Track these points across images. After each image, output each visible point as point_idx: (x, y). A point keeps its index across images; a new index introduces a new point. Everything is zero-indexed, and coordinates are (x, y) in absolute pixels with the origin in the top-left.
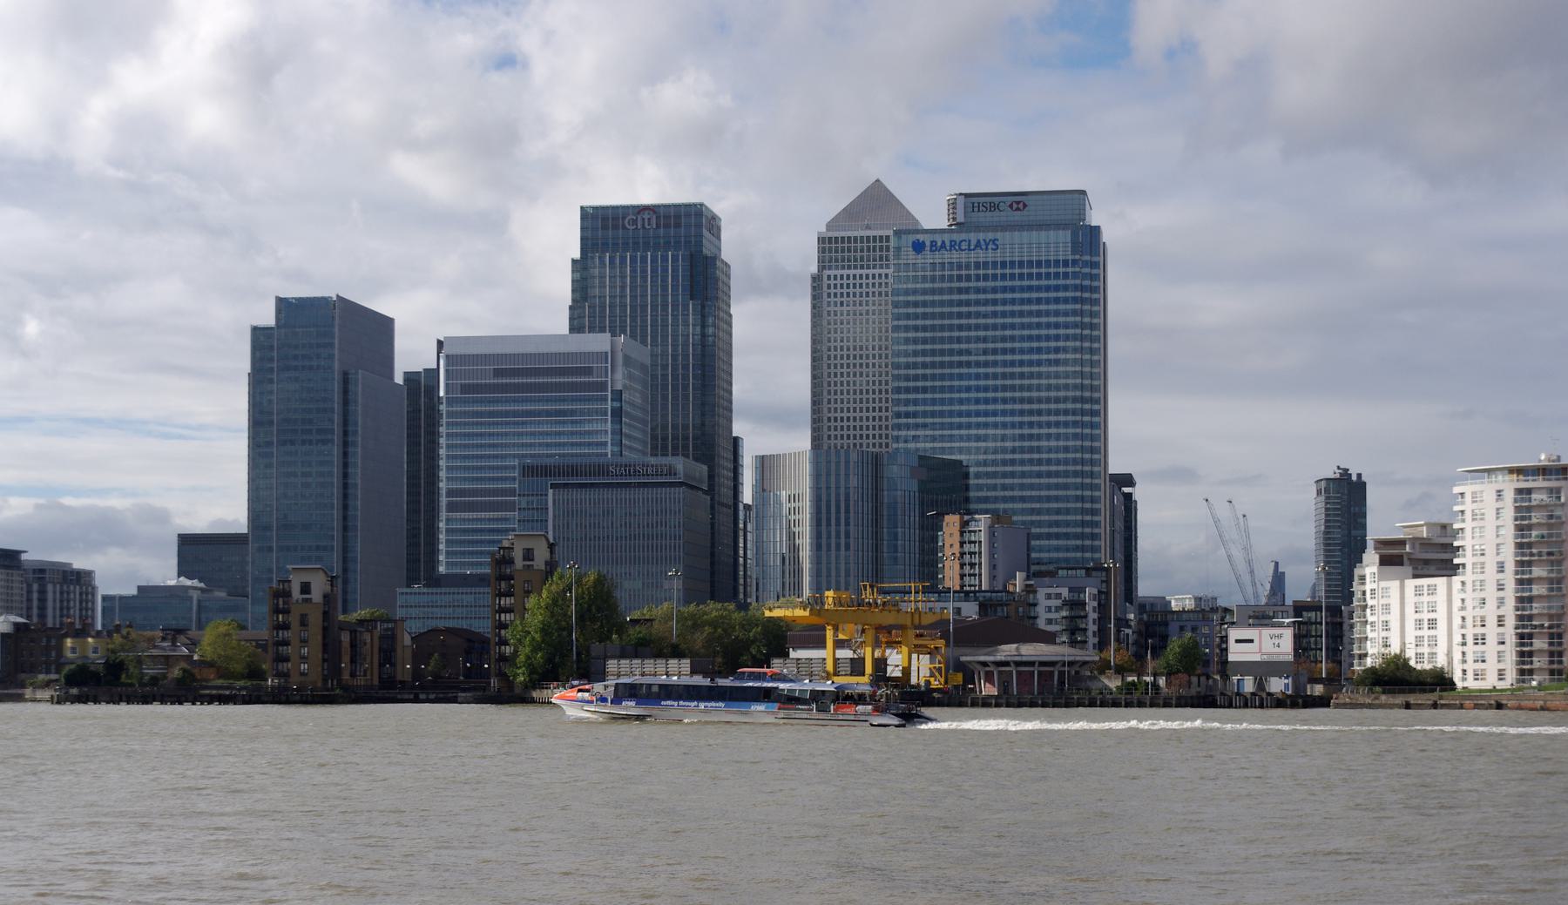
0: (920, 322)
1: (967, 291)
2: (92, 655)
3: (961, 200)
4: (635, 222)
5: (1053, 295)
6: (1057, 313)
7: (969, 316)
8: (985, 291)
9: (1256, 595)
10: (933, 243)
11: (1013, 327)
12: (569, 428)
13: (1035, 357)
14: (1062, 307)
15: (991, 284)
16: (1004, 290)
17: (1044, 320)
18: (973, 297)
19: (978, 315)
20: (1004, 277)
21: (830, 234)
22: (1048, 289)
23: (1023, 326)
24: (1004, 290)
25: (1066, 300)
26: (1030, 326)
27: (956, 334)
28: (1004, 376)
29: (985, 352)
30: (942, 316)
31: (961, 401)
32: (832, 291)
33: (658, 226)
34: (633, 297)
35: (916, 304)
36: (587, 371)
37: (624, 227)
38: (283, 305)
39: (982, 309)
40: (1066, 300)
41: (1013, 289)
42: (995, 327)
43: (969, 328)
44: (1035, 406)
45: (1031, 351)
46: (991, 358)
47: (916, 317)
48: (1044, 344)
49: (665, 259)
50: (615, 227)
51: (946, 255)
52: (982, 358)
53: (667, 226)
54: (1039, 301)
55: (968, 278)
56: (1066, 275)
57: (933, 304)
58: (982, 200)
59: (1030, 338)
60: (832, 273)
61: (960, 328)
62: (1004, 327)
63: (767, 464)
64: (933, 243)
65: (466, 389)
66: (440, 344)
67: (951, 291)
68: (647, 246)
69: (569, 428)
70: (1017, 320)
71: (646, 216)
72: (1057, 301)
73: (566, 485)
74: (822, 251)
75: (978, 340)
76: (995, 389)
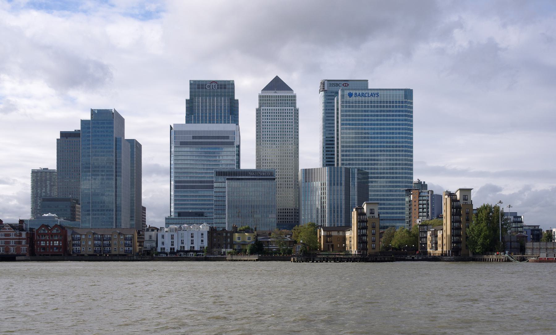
0: (351, 122)
1: (367, 111)
2: (247, 240)
3: (326, 82)
4: (209, 86)
5: (398, 113)
7: (368, 120)
10: (356, 94)
13: (391, 136)
14: (401, 118)
15: (376, 109)
16: (381, 111)
17: (395, 122)
18: (370, 113)
19: (371, 120)
20: (381, 106)
21: (263, 94)
22: (396, 111)
23: (387, 124)
24: (381, 111)
25: (402, 116)
27: (364, 127)
28: (381, 142)
29: (374, 133)
30: (359, 120)
32: (264, 114)
33: (218, 88)
34: (210, 114)
36: (228, 137)
37: (206, 88)
39: (373, 118)
40: (402, 116)
41: (384, 111)
43: (368, 124)
45: (390, 133)
46: (376, 136)
47: (350, 120)
49: (213, 100)
51: (360, 98)
52: (373, 136)
54: (393, 116)
55: (368, 107)
58: (333, 82)
59: (390, 129)
61: (365, 124)
63: (307, 172)
64: (356, 94)
66: (171, 128)
67: (362, 111)
70: (385, 122)
71: (214, 85)
74: (260, 100)
75: (372, 129)
76: (377, 147)
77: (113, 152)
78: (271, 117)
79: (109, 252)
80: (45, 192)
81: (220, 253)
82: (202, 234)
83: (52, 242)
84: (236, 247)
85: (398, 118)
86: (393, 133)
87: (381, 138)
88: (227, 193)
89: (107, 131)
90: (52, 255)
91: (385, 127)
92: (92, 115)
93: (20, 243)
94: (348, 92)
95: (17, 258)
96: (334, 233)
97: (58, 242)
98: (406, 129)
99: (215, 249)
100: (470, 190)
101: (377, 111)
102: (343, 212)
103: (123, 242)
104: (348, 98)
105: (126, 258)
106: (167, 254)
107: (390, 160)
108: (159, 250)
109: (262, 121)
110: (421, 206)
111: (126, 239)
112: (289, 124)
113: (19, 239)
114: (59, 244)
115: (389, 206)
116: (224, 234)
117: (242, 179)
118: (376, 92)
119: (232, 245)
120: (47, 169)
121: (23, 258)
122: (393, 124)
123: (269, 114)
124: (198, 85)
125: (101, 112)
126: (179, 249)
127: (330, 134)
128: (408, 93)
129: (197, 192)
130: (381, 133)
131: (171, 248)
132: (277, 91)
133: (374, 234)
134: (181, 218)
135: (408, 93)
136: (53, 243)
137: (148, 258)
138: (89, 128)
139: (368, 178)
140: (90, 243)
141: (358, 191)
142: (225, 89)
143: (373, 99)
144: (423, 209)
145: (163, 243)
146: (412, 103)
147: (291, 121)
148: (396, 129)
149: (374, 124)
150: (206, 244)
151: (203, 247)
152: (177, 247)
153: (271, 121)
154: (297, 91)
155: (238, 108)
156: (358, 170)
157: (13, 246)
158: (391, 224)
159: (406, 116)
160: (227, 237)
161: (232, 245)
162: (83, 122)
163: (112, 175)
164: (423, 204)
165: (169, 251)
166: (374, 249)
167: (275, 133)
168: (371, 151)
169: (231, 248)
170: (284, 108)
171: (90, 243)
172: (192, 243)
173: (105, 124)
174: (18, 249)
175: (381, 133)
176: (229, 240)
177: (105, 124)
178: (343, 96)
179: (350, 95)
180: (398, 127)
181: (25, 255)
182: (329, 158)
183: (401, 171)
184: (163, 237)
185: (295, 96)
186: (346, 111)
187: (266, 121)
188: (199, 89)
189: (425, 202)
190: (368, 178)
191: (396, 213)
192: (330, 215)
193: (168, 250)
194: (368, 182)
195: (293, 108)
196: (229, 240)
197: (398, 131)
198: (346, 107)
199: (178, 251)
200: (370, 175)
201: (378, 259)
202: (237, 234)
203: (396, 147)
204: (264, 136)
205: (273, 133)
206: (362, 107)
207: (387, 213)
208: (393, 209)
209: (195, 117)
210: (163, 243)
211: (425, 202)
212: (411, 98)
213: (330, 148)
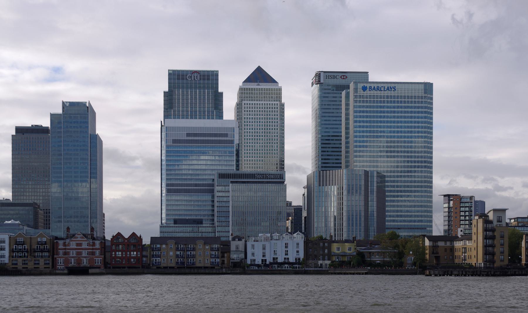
4: (191, 77)
6: (418, 117)
7: (384, 117)
8: (390, 107)
14: (420, 115)
18: (386, 109)
19: (388, 117)
21: (244, 87)
22: (415, 107)
23: (405, 122)
25: (422, 112)
26: (408, 122)
29: (390, 132)
32: (246, 109)
33: (200, 79)
36: (226, 135)
37: (186, 79)
38: (222, 93)
40: (422, 112)
41: (401, 107)
42: (394, 122)
43: (384, 122)
44: (409, 154)
45: (408, 132)
46: (392, 134)
48: (413, 130)
49: (204, 93)
53: (204, 79)
54: (411, 112)
55: (384, 102)
57: (363, 112)
59: (408, 127)
60: (246, 102)
62: (415, 122)
65: (175, 141)
68: (196, 88)
71: (195, 75)
72: (418, 112)
75: (388, 127)
77: (87, 150)
78: (253, 113)
79: (194, 264)
81: (316, 266)
82: (298, 244)
83: (128, 253)
84: (334, 259)
85: (417, 115)
86: (411, 132)
88: (230, 198)
89: (81, 127)
90: (129, 268)
91: (403, 125)
92: (63, 108)
93: (93, 254)
95: (91, 271)
96: (441, 244)
97: (135, 253)
98: (425, 127)
99: (310, 261)
101: (394, 107)
102: (363, 219)
103: (208, 253)
104: (361, 92)
105: (214, 271)
106: (258, 266)
107: (408, 162)
108: (249, 262)
109: (243, 116)
110: (462, 214)
112: (273, 120)
113: (93, 249)
114: (137, 254)
115: (407, 214)
116: (321, 244)
117: (248, 182)
118: (393, 85)
119: (330, 256)
121: (97, 271)
122: (411, 122)
123: (271, 110)
125: (73, 104)
126: (272, 261)
127: (325, 132)
128: (428, 87)
130: (398, 132)
131: (262, 260)
132: (260, 84)
133: (502, 245)
134: (177, 225)
136: (115, 254)
137: (238, 271)
139: (385, 182)
140: (171, 253)
141: (377, 197)
142: (208, 80)
144: (465, 216)
145: (253, 254)
147: (276, 117)
148: (415, 127)
149: (391, 122)
150: (302, 256)
151: (299, 259)
152: (269, 260)
153: (253, 116)
156: (378, 173)
157: (85, 257)
159: (425, 112)
160: (324, 248)
161: (330, 256)
162: (53, 117)
163: (87, 177)
164: (465, 212)
165: (260, 263)
166: (502, 261)
167: (258, 131)
169: (329, 260)
170: (269, 102)
171: (171, 253)
172: (287, 254)
173: (77, 119)
174: (91, 261)
175: (398, 132)
176: (326, 251)
177: (77, 119)
178: (356, 90)
179: (364, 89)
180: (417, 125)
181: (99, 268)
182: (325, 159)
183: (420, 174)
184: (253, 246)
185: (280, 89)
187: (248, 117)
188: (177, 78)
189: (467, 209)
190: (385, 182)
191: (415, 221)
193: (259, 261)
195: (278, 102)
196: (326, 251)
197: (417, 130)
198: (360, 102)
199: (271, 263)
200: (386, 179)
201: (517, 273)
202: (335, 244)
204: (246, 134)
205: (256, 131)
206: (377, 103)
207: (404, 221)
208: (411, 216)
209: (174, 111)
210: (253, 254)
211: (467, 209)
212: (431, 92)
213: (326, 148)
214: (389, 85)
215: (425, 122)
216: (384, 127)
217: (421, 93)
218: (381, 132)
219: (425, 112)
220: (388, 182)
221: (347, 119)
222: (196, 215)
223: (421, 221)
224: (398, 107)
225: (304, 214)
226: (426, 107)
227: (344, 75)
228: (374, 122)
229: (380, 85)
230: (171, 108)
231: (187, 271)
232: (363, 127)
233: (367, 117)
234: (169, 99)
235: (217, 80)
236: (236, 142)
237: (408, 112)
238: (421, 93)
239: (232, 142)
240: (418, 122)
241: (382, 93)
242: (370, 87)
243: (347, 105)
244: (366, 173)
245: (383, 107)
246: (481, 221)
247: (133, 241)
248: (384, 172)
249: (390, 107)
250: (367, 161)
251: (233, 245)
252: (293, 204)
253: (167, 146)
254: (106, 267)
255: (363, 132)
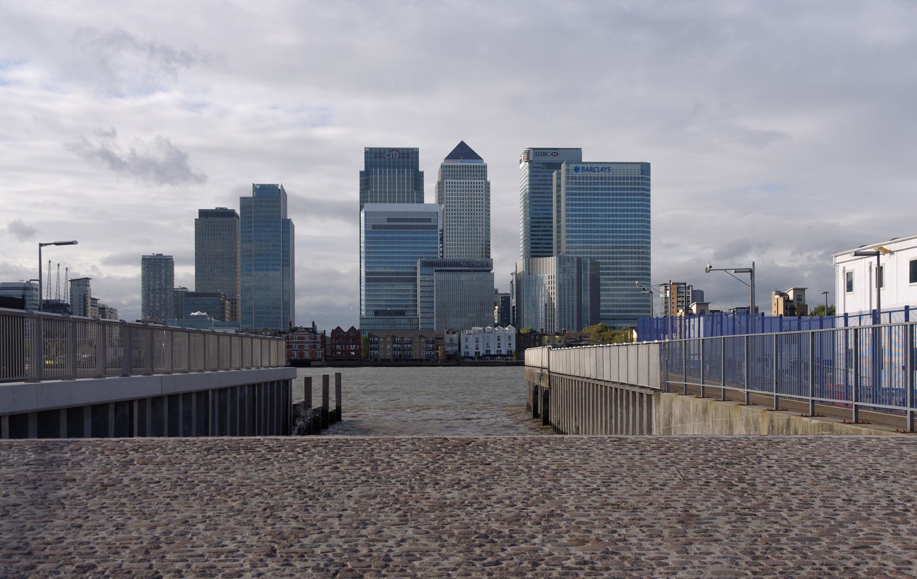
4: (389, 155)
6: (635, 200)
7: (598, 200)
8: (605, 189)
9: (58, 294)
11: (616, 205)
12: (383, 245)
14: (637, 197)
22: (631, 189)
25: (638, 195)
26: (624, 205)
28: (613, 226)
29: (605, 216)
31: (595, 237)
35: (576, 194)
36: (429, 220)
40: (638, 195)
41: (616, 189)
45: (624, 216)
50: (380, 157)
53: (403, 158)
55: (598, 183)
56: (638, 184)
57: (576, 194)
59: (624, 210)
62: (631, 205)
65: (374, 227)
68: (394, 167)
69: (383, 245)
73: (441, 271)
79: (410, 356)
80: (160, 284)
86: (627, 216)
87: (613, 221)
90: (349, 360)
93: (314, 347)
94: (574, 165)
95: (312, 363)
100: (804, 290)
101: (609, 189)
102: (575, 309)
104: (574, 174)
106: (472, 358)
108: (463, 354)
111: (427, 342)
116: (532, 337)
118: (607, 166)
120: (161, 255)
121: (318, 363)
122: (627, 205)
124: (376, 153)
125: (263, 187)
128: (645, 168)
129: (393, 286)
135: (645, 168)
138: (251, 207)
140: (388, 347)
142: (406, 160)
143: (603, 174)
146: (649, 180)
148: (631, 210)
149: (605, 205)
152: (482, 352)
154: (486, 160)
155: (423, 181)
158: (611, 325)
168: (602, 237)
171: (388, 347)
174: (312, 353)
178: (568, 170)
179: (577, 170)
184: (467, 340)
185: (485, 167)
186: (572, 189)
191: (631, 311)
192: (560, 317)
194: (599, 274)
203: (631, 232)
207: (621, 311)
209: (371, 192)
210: (467, 347)
212: (649, 173)
214: (604, 166)
215: (642, 205)
216: (598, 210)
217: (638, 174)
218: (594, 216)
219: (642, 194)
220: (602, 269)
221: (559, 201)
222: (398, 306)
223: (639, 311)
224: (613, 189)
225: (513, 302)
226: (643, 189)
227: (555, 152)
228: (587, 205)
229: (592, 166)
230: (368, 189)
231: (404, 363)
232: (576, 210)
233: (580, 200)
234: (365, 177)
235: (417, 158)
236: (440, 227)
237: (623, 194)
238: (638, 174)
239: (436, 227)
240: (635, 205)
241: (596, 174)
242: (583, 168)
243: (559, 186)
244: (579, 260)
245: (597, 189)
246: (781, 300)
247: (352, 334)
248: (598, 258)
249: (605, 189)
250: (580, 248)
251: (447, 338)
252: (499, 292)
253: (366, 232)
254: (326, 360)
255: (576, 216)
